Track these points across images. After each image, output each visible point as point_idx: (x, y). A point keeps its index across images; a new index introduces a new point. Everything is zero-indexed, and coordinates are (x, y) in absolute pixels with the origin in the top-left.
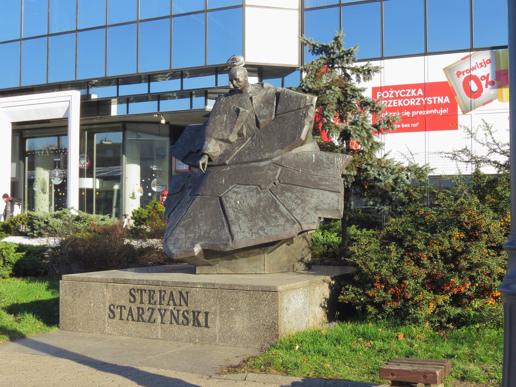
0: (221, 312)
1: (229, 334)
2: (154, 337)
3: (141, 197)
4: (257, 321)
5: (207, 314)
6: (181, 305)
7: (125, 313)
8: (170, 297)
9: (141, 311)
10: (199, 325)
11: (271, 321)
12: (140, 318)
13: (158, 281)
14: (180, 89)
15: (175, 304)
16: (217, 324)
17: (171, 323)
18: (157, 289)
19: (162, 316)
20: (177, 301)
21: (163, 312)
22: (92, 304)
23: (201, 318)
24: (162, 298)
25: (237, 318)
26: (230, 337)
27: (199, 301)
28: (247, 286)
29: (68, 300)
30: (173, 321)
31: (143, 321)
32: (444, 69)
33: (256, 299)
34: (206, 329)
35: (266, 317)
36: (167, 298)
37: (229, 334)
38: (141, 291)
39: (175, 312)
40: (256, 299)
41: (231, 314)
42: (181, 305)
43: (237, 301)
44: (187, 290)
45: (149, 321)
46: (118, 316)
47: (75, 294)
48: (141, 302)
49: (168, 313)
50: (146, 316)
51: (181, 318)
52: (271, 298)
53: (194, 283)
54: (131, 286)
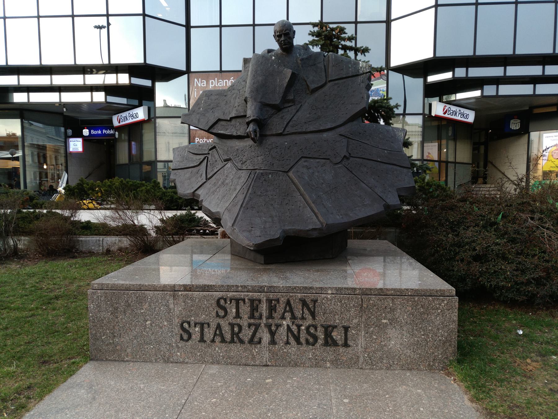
0: (367, 326)
1: (379, 354)
2: (257, 363)
3: (14, 134)
4: (423, 335)
5: (346, 329)
6: (303, 318)
7: (209, 334)
8: (286, 308)
9: (236, 329)
10: (335, 343)
11: (446, 334)
12: (236, 338)
13: (261, 287)
14: (192, 25)
15: (293, 317)
16: (360, 342)
17: (287, 343)
18: (263, 297)
19: (272, 334)
20: (298, 314)
21: (273, 328)
22: (148, 322)
23: (337, 335)
24: (272, 309)
25: (392, 333)
26: (381, 358)
27: (332, 312)
28: (407, 290)
29: (105, 318)
30: (292, 341)
31: (242, 342)
32: (244, 59)
33: (422, 306)
34: (341, 350)
35: (438, 329)
36: (280, 308)
37: (379, 354)
38: (237, 301)
39: (294, 328)
40: (422, 306)
41: (382, 328)
42: (303, 318)
43: (392, 310)
44: (312, 296)
45: (251, 341)
46: (196, 336)
47: (116, 309)
48: (238, 315)
49: (283, 331)
50: (246, 334)
51: (303, 336)
52: (447, 304)
53: (321, 288)
54: (219, 294)
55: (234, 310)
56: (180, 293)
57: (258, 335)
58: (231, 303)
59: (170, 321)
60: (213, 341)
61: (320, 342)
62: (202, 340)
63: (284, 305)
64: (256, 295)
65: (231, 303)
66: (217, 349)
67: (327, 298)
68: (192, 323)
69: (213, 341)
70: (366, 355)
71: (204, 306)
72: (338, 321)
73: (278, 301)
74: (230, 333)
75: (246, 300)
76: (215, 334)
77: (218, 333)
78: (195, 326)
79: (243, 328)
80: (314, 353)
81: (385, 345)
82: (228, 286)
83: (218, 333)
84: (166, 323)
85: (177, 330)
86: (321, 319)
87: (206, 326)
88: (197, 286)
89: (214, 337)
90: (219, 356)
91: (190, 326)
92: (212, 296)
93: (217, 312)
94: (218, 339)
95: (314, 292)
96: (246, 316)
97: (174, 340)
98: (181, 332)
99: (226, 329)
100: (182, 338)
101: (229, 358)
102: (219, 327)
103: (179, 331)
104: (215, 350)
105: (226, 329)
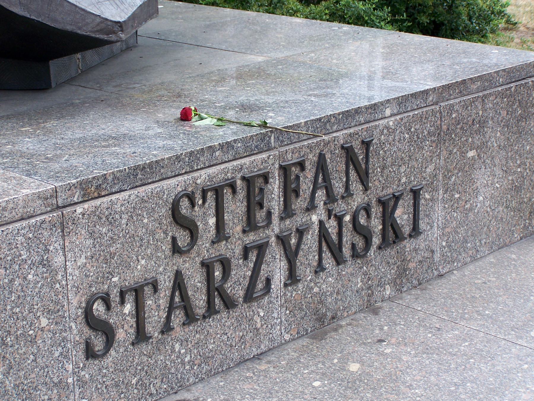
7: (156, 308)
20: (338, 187)
24: (290, 191)
49: (311, 239)
54: (174, 185)
55: (212, 221)
56: (79, 209)
57: (263, 274)
58: (204, 202)
59: (54, 311)
60: (167, 328)
61: (376, 241)
62: (141, 335)
63: (314, 170)
64: (251, 163)
65: (204, 202)
66: (177, 346)
67: (387, 127)
68: (115, 296)
69: (167, 328)
70: (444, 244)
71: (141, 232)
72: (404, 180)
73: (301, 165)
74: (204, 291)
75: (239, 182)
76: (171, 309)
77: (177, 299)
78: (123, 302)
79: (234, 262)
80: (365, 274)
81: (471, 210)
82: (191, 153)
83: (177, 299)
84: (44, 322)
85: (77, 331)
86: (379, 187)
87: (148, 290)
88: (115, 178)
89: (168, 318)
90: (183, 363)
91: (108, 307)
92: (159, 195)
93: (174, 239)
94: (178, 317)
95: (362, 120)
96: (239, 228)
97: (70, 367)
98: (87, 331)
99: (195, 281)
100: (90, 353)
101: (206, 359)
102: (179, 283)
103: (81, 332)
104: (173, 351)
105: (195, 281)
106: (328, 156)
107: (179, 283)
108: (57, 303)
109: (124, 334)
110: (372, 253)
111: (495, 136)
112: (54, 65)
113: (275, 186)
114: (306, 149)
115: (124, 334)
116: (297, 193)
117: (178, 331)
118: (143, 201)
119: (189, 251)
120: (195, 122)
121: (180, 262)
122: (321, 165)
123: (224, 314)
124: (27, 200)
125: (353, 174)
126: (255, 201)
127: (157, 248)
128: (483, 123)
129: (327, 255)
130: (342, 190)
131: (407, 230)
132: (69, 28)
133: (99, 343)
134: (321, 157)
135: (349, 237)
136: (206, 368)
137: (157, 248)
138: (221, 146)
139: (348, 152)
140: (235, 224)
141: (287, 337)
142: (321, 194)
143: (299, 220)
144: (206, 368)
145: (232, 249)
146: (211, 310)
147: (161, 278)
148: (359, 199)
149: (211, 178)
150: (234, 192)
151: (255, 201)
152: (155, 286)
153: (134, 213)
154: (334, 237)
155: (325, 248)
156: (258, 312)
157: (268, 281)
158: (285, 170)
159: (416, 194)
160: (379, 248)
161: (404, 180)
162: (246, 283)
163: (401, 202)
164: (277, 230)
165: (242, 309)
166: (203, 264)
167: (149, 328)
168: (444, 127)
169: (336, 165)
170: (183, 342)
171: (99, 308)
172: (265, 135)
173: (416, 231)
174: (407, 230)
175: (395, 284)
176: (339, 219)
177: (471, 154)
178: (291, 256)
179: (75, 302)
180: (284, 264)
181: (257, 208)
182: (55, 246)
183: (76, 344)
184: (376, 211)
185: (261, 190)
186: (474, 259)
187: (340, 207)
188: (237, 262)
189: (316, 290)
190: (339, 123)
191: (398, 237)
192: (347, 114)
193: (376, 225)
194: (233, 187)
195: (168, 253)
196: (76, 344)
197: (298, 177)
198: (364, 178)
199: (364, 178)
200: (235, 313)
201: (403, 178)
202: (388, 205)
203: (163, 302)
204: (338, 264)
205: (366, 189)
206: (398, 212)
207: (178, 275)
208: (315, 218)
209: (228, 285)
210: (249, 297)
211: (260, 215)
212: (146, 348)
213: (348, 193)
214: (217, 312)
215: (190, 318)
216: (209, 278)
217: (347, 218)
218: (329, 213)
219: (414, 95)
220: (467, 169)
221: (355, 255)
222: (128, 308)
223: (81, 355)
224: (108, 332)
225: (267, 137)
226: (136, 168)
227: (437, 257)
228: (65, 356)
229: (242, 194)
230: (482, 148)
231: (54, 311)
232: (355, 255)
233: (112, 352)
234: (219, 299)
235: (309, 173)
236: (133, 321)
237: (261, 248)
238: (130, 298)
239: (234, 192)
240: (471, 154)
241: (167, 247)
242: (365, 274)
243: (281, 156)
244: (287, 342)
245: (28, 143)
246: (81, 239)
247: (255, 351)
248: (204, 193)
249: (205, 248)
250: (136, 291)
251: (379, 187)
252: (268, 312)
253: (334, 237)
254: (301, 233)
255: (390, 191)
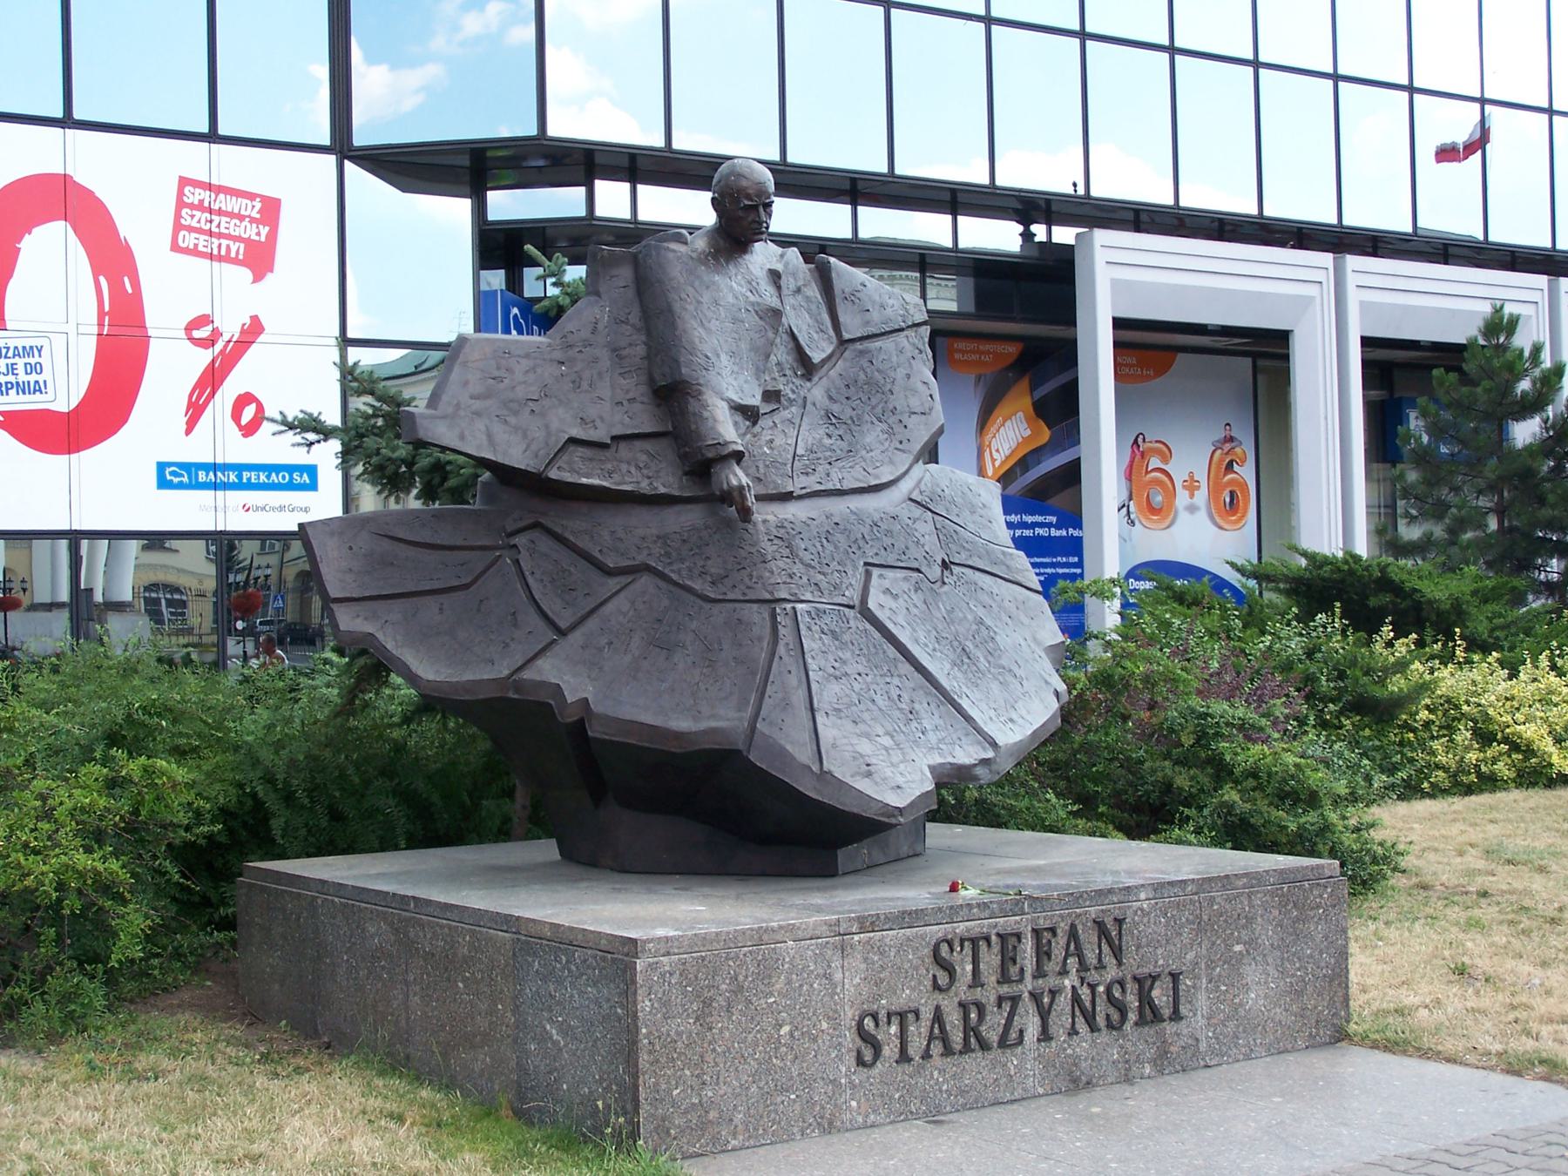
20: (1091, 957)
24: (1043, 953)
49: (1064, 1001)
54: (936, 931)
55: (969, 968)
56: (856, 938)
59: (833, 1019)
60: (927, 1055)
61: (1132, 1017)
62: (904, 1057)
64: (1008, 923)
66: (936, 1074)
67: (1142, 910)
68: (882, 1015)
69: (927, 1055)
72: (1161, 962)
73: (1053, 931)
75: (994, 938)
76: (931, 1038)
78: (889, 1023)
79: (988, 1008)
80: (1121, 1047)
81: (1241, 1004)
83: (936, 1031)
84: (825, 1025)
85: (850, 1039)
86: (1133, 963)
87: (911, 1016)
89: (928, 1045)
91: (877, 1025)
94: (937, 1048)
96: (993, 979)
98: (858, 1040)
99: (953, 1018)
100: (860, 1062)
101: (962, 1092)
102: (938, 1017)
105: (953, 1018)
106: (1080, 928)
107: (938, 1017)
108: (836, 1011)
109: (890, 1050)
110: (1128, 1026)
111: (1266, 934)
112: (842, 854)
113: (1028, 945)
114: (1060, 918)
115: (890, 1050)
116: (1049, 955)
117: (937, 1060)
118: (909, 939)
119: (948, 989)
120: (962, 892)
121: (939, 998)
122: (1073, 934)
123: (980, 1054)
124: (816, 925)
125: (1105, 947)
126: (1008, 957)
127: (920, 983)
128: (1250, 920)
129: (1080, 1020)
130: (1095, 961)
131: (1166, 1012)
132: (855, 811)
133: (868, 1055)
134: (1073, 926)
135: (1102, 1008)
136: (961, 1101)
137: (920, 983)
138: (978, 905)
139: (1100, 925)
140: (990, 976)
141: (1041, 1091)
142: (1072, 962)
143: (1052, 981)
144: (961, 1101)
145: (988, 995)
146: (966, 1049)
147: (922, 1009)
148: (1112, 973)
149: (968, 930)
150: (989, 945)
151: (1008, 957)
152: (917, 1013)
153: (900, 948)
154: (1088, 1004)
155: (1078, 1013)
156: (1013, 1060)
157: (1021, 1032)
158: (1037, 933)
159: (1175, 977)
160: (1136, 1024)
161: (1161, 962)
162: (1001, 1030)
163: (1157, 983)
164: (1030, 987)
165: (996, 1053)
166: (961, 1004)
167: (911, 1052)
168: (1205, 918)
169: (1089, 938)
170: (942, 1071)
171: (868, 1022)
172: (1018, 902)
173: (1176, 1016)
174: (1166, 1012)
175: (1155, 1065)
176: (1092, 987)
177: (1238, 948)
178: (1044, 1014)
179: (850, 1014)
180: (1037, 1020)
181: (1010, 964)
182: (836, 964)
183: (850, 1050)
184: (1131, 987)
185: (1015, 948)
186: (1248, 1058)
187: (1093, 976)
188: (991, 1008)
189: (1069, 1051)
190: (1091, 899)
191: (1157, 1017)
192: (1100, 893)
193: (1132, 1001)
194: (987, 939)
195: (930, 988)
196: (850, 1050)
197: (1049, 942)
198: (1117, 953)
199: (1117, 953)
200: (991, 1055)
201: (1161, 961)
202: (1144, 984)
203: (924, 1031)
204: (1092, 1031)
205: (1120, 964)
206: (1155, 993)
207: (938, 1008)
208: (1067, 982)
209: (983, 1028)
210: (1003, 1043)
211: (1013, 971)
212: (908, 1069)
213: (1101, 966)
214: (973, 1051)
215: (948, 1051)
216: (966, 1018)
217: (1101, 989)
218: (1082, 980)
219: (1171, 884)
220: (1234, 963)
221: (1110, 1026)
222: (894, 1029)
223: (853, 1062)
224: (877, 1048)
225: (1019, 902)
226: (904, 912)
227: (1203, 1046)
228: (840, 1058)
229: (996, 948)
230: (1251, 943)
231: (833, 1019)
232: (1110, 1026)
233: (878, 1064)
234: (974, 1040)
235: (1061, 939)
236: (898, 1042)
237: (1015, 1000)
238: (895, 1020)
239: (989, 945)
240: (1238, 948)
241: (928, 983)
242: (1121, 1047)
243: (1033, 920)
244: (1040, 1096)
245: (818, 899)
246: (856, 961)
247: (1008, 1096)
248: (962, 941)
249: (962, 990)
250: (900, 1014)
251: (1133, 963)
252: (1022, 1061)
253: (1088, 1004)
254: (1053, 993)
255: (1146, 970)
